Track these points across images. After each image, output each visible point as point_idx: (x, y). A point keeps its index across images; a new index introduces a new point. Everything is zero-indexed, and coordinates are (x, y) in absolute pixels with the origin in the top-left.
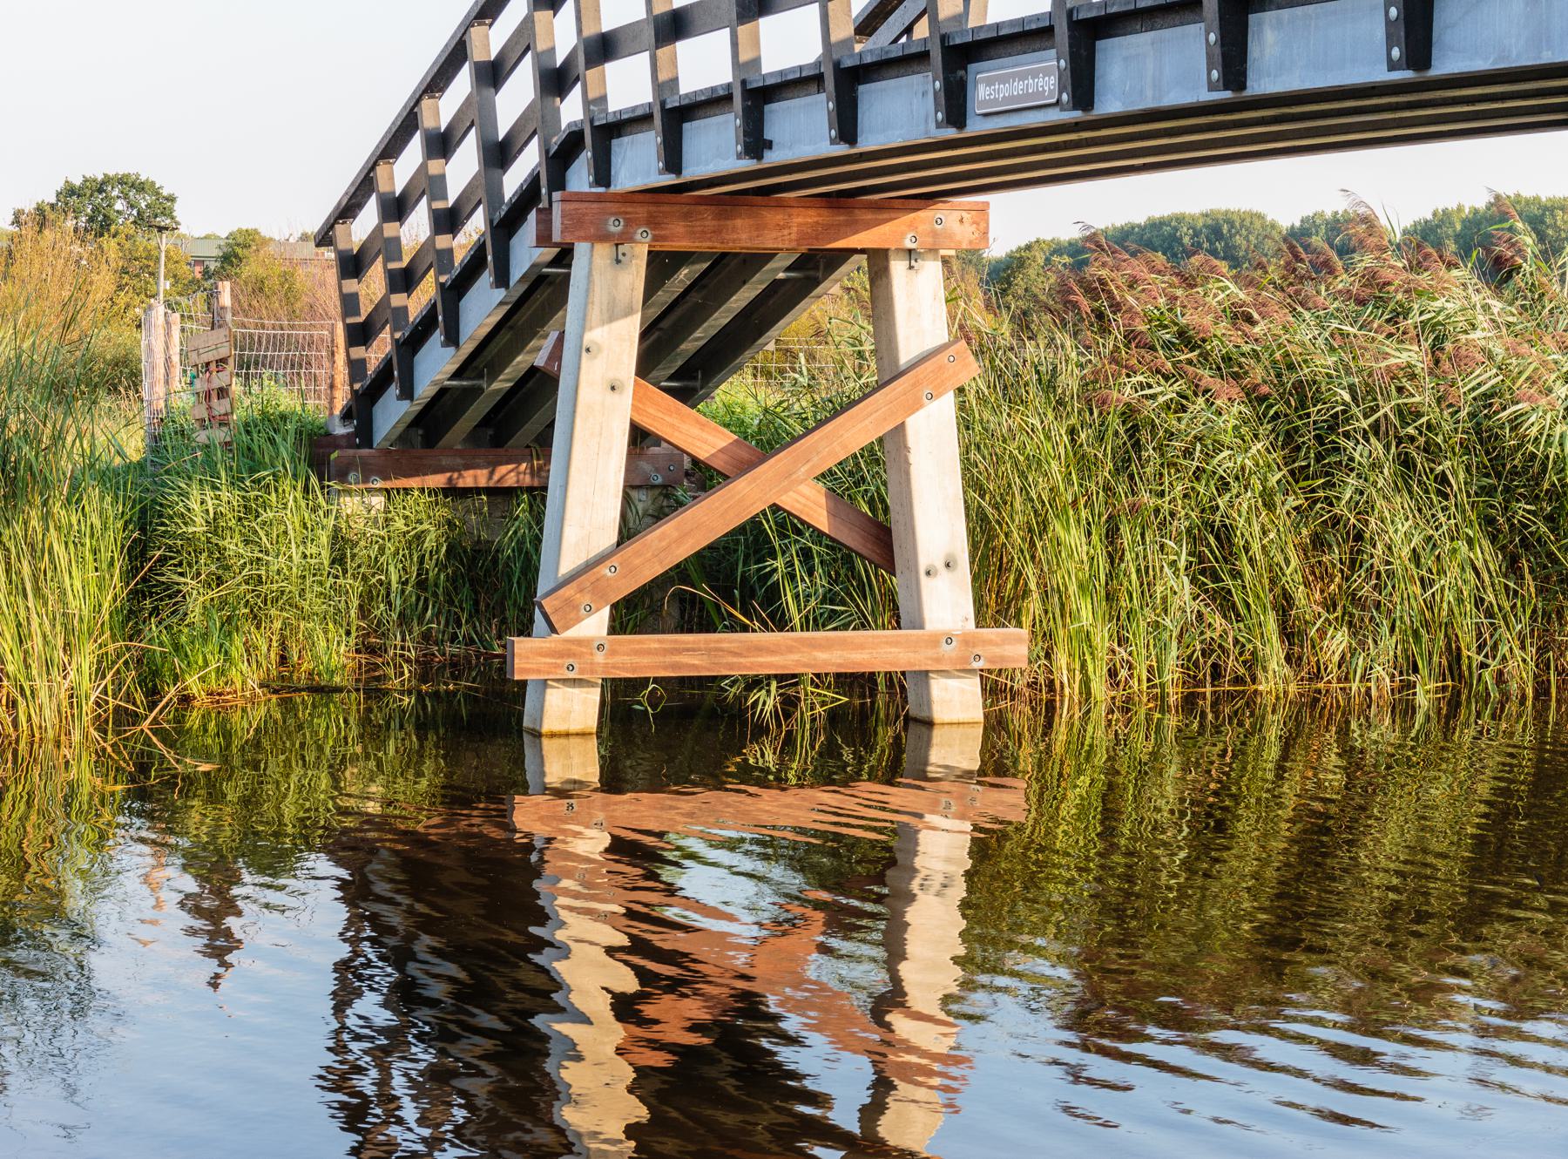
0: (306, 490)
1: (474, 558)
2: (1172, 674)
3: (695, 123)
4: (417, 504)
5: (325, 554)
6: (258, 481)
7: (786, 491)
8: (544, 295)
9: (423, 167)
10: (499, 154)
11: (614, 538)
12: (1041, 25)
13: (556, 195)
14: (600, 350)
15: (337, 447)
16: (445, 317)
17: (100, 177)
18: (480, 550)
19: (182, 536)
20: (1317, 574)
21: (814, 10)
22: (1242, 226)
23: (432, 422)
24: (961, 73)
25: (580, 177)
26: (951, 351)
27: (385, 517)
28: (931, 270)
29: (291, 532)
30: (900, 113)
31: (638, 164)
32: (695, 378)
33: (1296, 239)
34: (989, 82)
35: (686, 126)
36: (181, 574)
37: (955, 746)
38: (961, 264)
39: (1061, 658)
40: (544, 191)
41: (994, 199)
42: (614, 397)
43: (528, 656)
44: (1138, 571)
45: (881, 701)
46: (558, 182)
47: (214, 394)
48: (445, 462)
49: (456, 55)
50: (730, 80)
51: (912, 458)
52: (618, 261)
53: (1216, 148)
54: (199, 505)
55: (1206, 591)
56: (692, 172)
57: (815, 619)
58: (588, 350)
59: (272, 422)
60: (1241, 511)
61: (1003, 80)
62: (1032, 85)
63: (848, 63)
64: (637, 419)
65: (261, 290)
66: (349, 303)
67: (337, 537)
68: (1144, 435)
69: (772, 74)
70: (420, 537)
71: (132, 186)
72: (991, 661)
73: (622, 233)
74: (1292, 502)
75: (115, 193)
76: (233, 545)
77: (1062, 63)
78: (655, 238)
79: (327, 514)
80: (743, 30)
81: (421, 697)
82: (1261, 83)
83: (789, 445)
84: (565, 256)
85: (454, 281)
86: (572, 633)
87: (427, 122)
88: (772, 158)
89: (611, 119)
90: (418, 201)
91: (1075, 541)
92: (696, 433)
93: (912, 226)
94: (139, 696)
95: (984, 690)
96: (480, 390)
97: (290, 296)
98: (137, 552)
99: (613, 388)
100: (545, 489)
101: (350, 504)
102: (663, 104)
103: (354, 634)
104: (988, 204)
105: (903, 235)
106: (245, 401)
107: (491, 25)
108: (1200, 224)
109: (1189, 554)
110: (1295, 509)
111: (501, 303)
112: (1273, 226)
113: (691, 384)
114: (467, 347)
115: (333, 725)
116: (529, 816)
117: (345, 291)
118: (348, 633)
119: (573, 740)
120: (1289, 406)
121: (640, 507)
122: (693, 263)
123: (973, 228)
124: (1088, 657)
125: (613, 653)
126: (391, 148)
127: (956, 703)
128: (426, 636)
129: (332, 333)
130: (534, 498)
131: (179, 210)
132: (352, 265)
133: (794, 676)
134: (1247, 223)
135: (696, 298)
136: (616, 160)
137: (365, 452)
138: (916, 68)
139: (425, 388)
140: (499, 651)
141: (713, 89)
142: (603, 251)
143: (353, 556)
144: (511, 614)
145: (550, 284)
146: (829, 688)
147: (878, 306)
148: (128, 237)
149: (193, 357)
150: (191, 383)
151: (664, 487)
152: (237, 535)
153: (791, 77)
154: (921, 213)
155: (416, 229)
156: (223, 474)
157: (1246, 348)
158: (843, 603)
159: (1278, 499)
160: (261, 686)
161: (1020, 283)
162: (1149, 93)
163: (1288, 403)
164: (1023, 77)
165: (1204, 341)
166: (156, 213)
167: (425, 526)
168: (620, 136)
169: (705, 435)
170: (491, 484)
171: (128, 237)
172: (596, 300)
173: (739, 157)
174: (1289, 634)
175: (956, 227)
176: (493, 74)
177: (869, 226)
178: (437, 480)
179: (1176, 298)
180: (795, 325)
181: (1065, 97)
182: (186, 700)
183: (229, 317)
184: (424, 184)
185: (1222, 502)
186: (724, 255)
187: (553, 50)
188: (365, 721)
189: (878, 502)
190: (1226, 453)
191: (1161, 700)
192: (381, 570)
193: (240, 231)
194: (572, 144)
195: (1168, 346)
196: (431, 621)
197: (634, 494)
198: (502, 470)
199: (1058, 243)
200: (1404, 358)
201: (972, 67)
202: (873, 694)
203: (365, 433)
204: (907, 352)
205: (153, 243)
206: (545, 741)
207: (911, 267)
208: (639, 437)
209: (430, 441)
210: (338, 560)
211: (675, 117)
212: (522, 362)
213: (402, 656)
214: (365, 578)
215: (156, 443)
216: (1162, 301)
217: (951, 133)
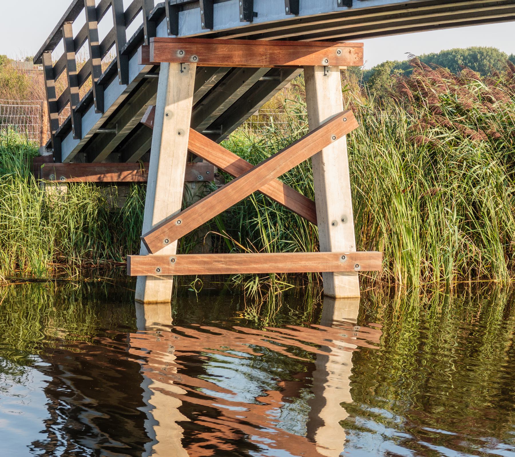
3: (220, 4)
4: (83, 190)
5: (38, 214)
6: (6, 178)
7: (263, 184)
8: (146, 88)
9: (86, 25)
11: (180, 207)
13: (152, 39)
14: (173, 115)
15: (44, 162)
16: (96, 99)
22: (487, 55)
23: (90, 150)
25: (163, 30)
26: (345, 116)
27: (67, 196)
37: (346, 311)
40: (145, 37)
41: (365, 41)
42: (180, 137)
43: (137, 264)
46: (153, 33)
51: (326, 168)
52: (182, 71)
53: (474, 17)
57: (278, 247)
58: (167, 115)
64: (192, 149)
65: (7, 85)
66: (50, 92)
67: (44, 206)
68: (439, 158)
70: (84, 206)
72: (364, 267)
73: (184, 58)
78: (200, 60)
79: (39, 195)
81: (85, 285)
83: (265, 161)
84: (156, 69)
85: (101, 81)
88: (258, 21)
92: (220, 156)
93: (325, 54)
97: (21, 89)
99: (179, 134)
100: (146, 182)
101: (51, 190)
103: (52, 254)
104: (363, 44)
105: (321, 59)
108: (466, 54)
111: (125, 92)
113: (217, 131)
115: (43, 297)
116: (136, 341)
118: (49, 253)
119: (159, 306)
120: (510, 143)
121: (192, 191)
122: (219, 72)
123: (356, 56)
124: (411, 266)
127: (346, 288)
129: (42, 106)
132: (52, 73)
133: (267, 274)
134: (489, 53)
135: (219, 89)
136: (181, 22)
137: (58, 164)
139: (87, 135)
143: (52, 217)
144: (129, 244)
145: (149, 82)
146: (284, 280)
147: (310, 94)
151: (204, 182)
154: (330, 49)
155: (83, 56)
157: (489, 115)
158: (291, 239)
161: (378, 83)
163: (509, 141)
165: (468, 111)
167: (87, 201)
168: (182, 10)
169: (224, 157)
170: (120, 180)
172: (171, 90)
173: (241, 20)
175: (347, 55)
178: (93, 179)
179: (455, 90)
180: (269, 103)
184: (87, 34)
186: (233, 69)
188: (58, 296)
195: (451, 113)
197: (190, 185)
198: (125, 173)
199: (397, 63)
202: (306, 284)
203: (58, 155)
206: (146, 307)
207: (325, 75)
208: (192, 157)
209: (90, 159)
210: (45, 217)
213: (76, 264)
214: (58, 227)
216: (448, 91)
217: (345, 9)
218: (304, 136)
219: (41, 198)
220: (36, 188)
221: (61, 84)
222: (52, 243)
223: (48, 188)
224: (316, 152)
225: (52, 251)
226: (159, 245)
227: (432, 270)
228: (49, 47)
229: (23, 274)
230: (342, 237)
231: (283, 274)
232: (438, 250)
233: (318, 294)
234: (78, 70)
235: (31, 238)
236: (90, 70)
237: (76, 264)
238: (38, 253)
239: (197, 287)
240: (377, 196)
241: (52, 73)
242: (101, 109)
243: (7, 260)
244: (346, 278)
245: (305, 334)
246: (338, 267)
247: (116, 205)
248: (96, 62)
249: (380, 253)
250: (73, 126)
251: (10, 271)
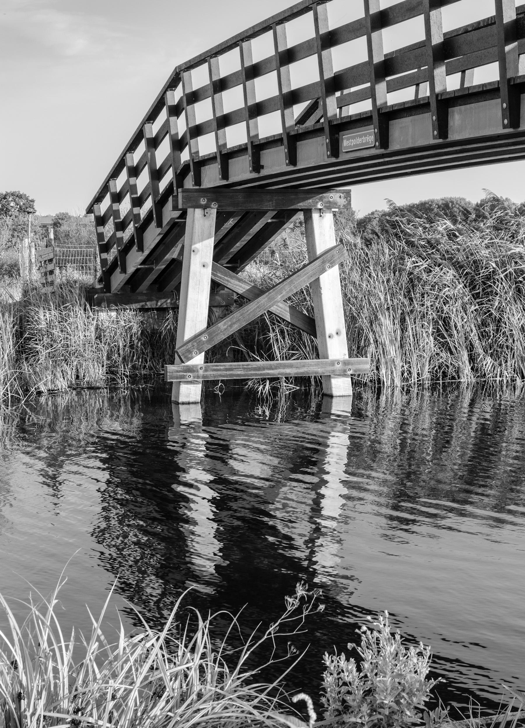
0: (85, 310)
1: (152, 336)
2: (426, 375)
3: (234, 160)
5: (93, 335)
6: (66, 307)
7: (273, 305)
8: (176, 231)
9: (128, 181)
10: (157, 175)
11: (205, 325)
12: (367, 115)
13: (180, 190)
14: (198, 251)
17: (4, 193)
18: (154, 332)
19: (37, 329)
20: (483, 336)
21: (460, 74)
24: (337, 136)
25: (189, 183)
27: (119, 322)
28: (329, 217)
29: (79, 327)
30: (313, 153)
31: (211, 177)
32: (237, 263)
33: (479, 207)
34: (348, 139)
35: (230, 161)
36: (37, 344)
37: (341, 406)
38: (342, 217)
39: (383, 371)
41: (353, 188)
44: (413, 335)
45: (312, 389)
47: (48, 273)
48: (140, 298)
49: (139, 136)
50: (247, 142)
51: (323, 291)
52: (205, 216)
54: (44, 317)
55: (440, 343)
56: (233, 179)
57: (286, 357)
59: (70, 284)
60: (453, 311)
61: (353, 138)
62: (364, 139)
63: (292, 133)
64: (214, 278)
66: (100, 236)
69: (263, 139)
70: (130, 328)
71: (17, 196)
72: (355, 371)
73: (206, 204)
74: (473, 308)
75: (10, 199)
76: (56, 332)
77: (376, 130)
78: (219, 206)
79: (93, 319)
80: (251, 122)
81: (132, 390)
82: (454, 136)
84: (184, 215)
86: (190, 363)
87: (129, 163)
88: (264, 172)
89: (200, 159)
90: (126, 194)
91: (387, 324)
92: (238, 285)
93: (321, 199)
94: (20, 392)
95: (352, 383)
96: (153, 269)
98: (19, 334)
99: (204, 266)
101: (103, 315)
102: (220, 152)
103: (105, 367)
104: (350, 191)
106: (59, 277)
107: (153, 123)
108: (440, 203)
109: (434, 328)
110: (475, 310)
111: (160, 234)
112: (469, 203)
113: (235, 265)
114: (147, 252)
115: (97, 402)
116: (173, 435)
117: (99, 231)
118: (103, 366)
119: (192, 406)
120: (472, 270)
121: (217, 314)
122: (235, 217)
123: (345, 200)
124: (394, 370)
125: (206, 370)
126: (115, 174)
127: (341, 387)
128: (134, 367)
130: (175, 312)
131: (36, 206)
132: (101, 221)
134: (459, 202)
135: (236, 230)
136: (203, 175)
137: (108, 294)
138: (319, 134)
139: (131, 269)
140: (162, 372)
141: (240, 146)
142: (198, 212)
143: (104, 336)
144: (167, 357)
145: (179, 226)
146: (291, 383)
148: (16, 217)
149: (40, 259)
150: (39, 269)
151: (226, 306)
152: (58, 328)
153: (270, 140)
155: (125, 206)
156: (52, 304)
158: (297, 350)
159: (468, 306)
160: (69, 387)
162: (410, 141)
163: (471, 268)
164: (361, 136)
166: (27, 208)
167: (132, 324)
168: (204, 166)
169: (240, 284)
171: (16, 217)
172: (197, 231)
173: (251, 172)
174: (472, 359)
175: (338, 200)
176: (154, 143)
177: (304, 200)
178: (138, 306)
180: (275, 241)
181: (377, 144)
182: (39, 393)
183: (53, 242)
184: (128, 188)
185: (445, 308)
187: (177, 134)
188: (111, 399)
189: (311, 310)
190: (447, 289)
191: (421, 385)
192: (115, 341)
193: (60, 213)
194: (186, 169)
195: (423, 247)
196: (135, 361)
197: (214, 309)
200: (517, 250)
201: (341, 133)
202: (309, 386)
203: (107, 287)
204: (320, 249)
205: (26, 219)
206: (180, 406)
207: (321, 216)
208: (215, 286)
210: (99, 338)
211: (226, 157)
212: (169, 257)
213: (124, 374)
214: (109, 344)
215: (25, 293)
217: (334, 160)
218: (305, 266)
219: (95, 322)
220: (91, 314)
221: (109, 230)
222: (105, 358)
223: (101, 314)
224: (314, 279)
225: (105, 364)
226: (190, 356)
227: (410, 373)
228: (98, 199)
229: (82, 383)
230: (337, 348)
231: (291, 377)
232: (415, 356)
233: (319, 394)
234: (122, 217)
235: (88, 354)
236: (131, 217)
237: (124, 374)
238: (94, 365)
239: (221, 390)
240: (366, 313)
241: (101, 221)
242: (141, 249)
243: (69, 373)
244: (191, 387)
245: (313, 428)
246: (334, 371)
247: (156, 327)
248: (136, 210)
249: (369, 359)
250: (120, 262)
251: (71, 381)
